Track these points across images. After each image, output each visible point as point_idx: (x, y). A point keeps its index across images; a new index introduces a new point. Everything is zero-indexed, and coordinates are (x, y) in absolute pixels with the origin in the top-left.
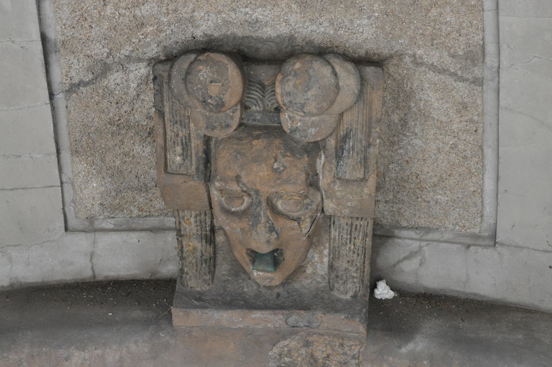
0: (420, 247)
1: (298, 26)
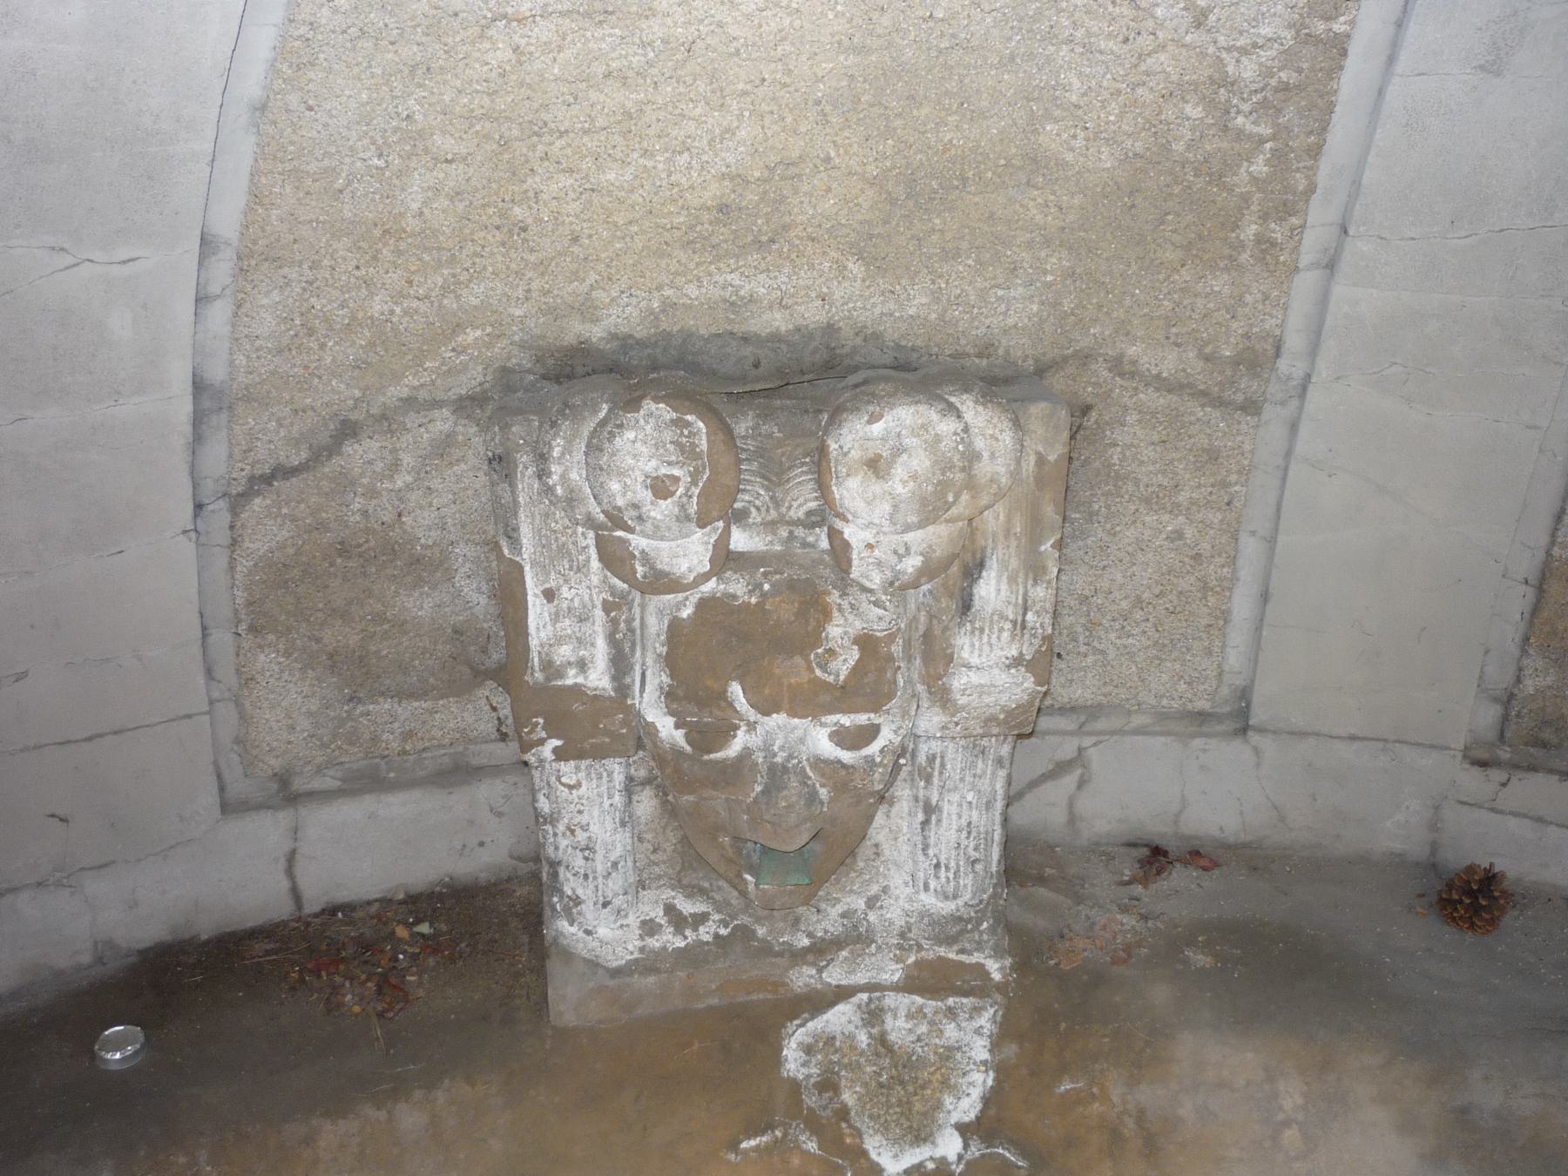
0: (1080, 750)
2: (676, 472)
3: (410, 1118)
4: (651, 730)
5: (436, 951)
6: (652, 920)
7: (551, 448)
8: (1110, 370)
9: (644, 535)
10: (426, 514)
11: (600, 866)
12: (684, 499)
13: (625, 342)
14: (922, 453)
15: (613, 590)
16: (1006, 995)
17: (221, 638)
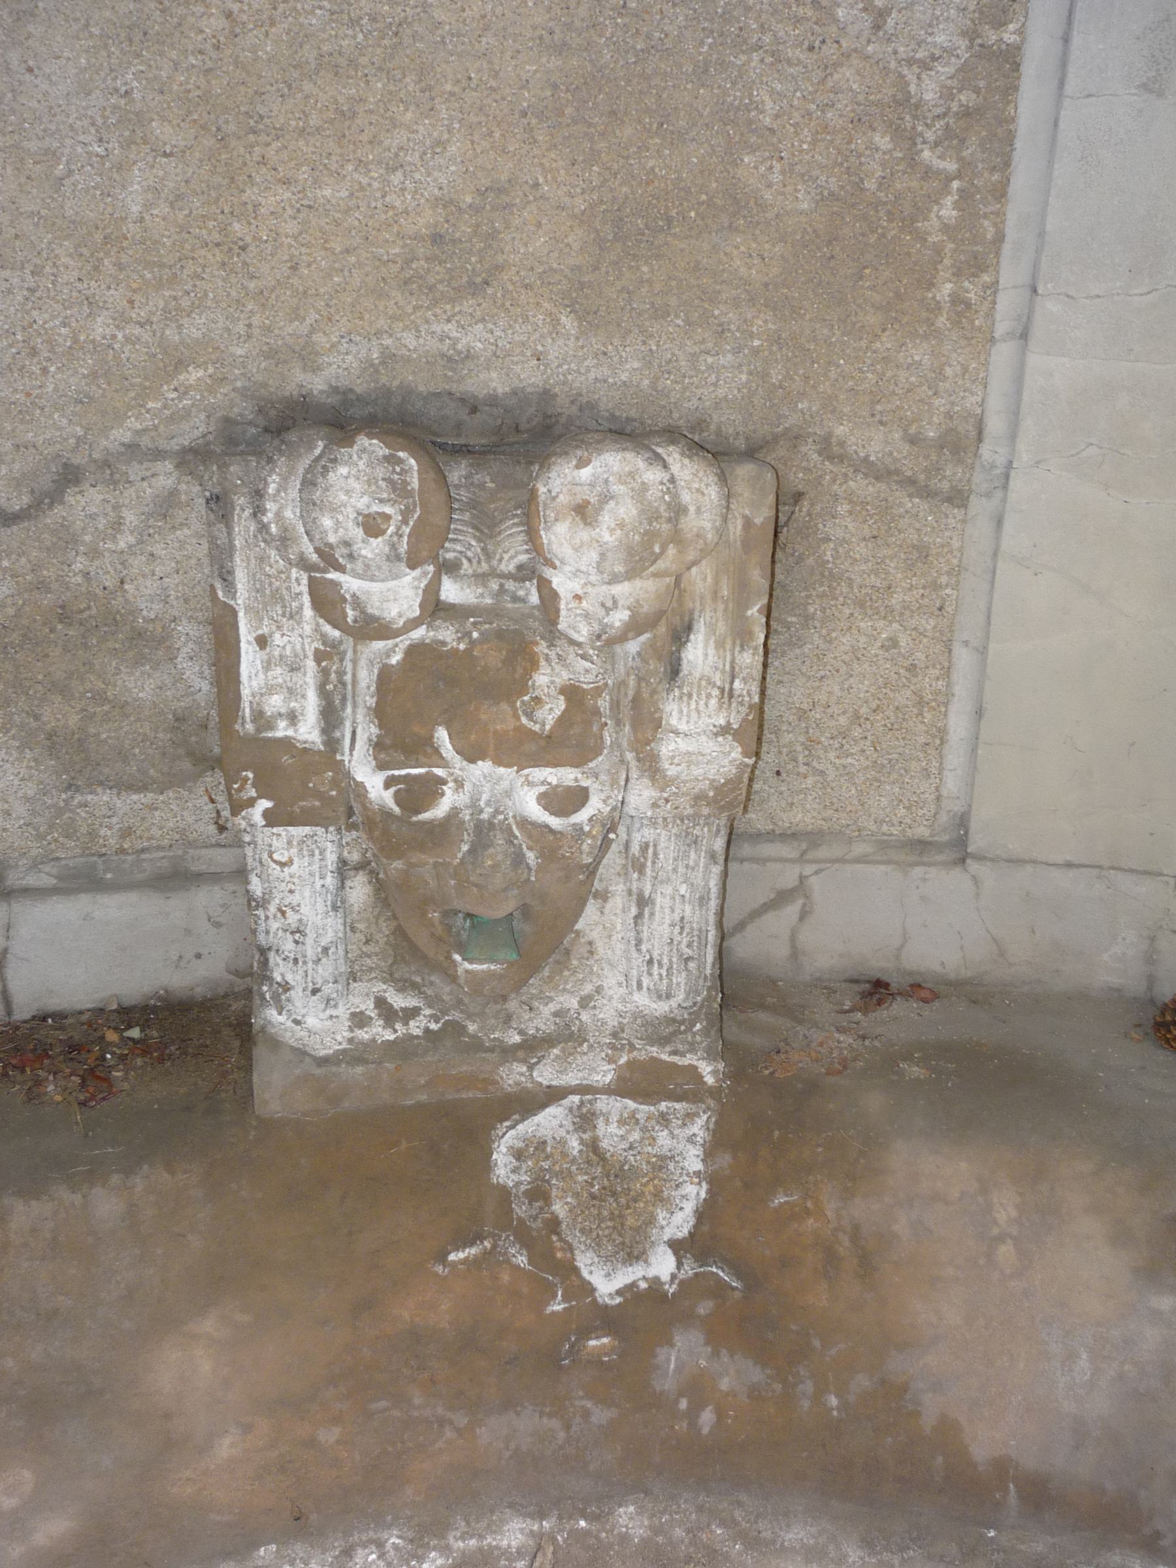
0: (802, 879)
1: (565, 367)
2: (388, 510)
3: (106, 1204)
5: (145, 1052)
6: (362, 1013)
7: (266, 484)
8: (820, 455)
9: (357, 575)
10: (148, 583)
11: (310, 951)
12: (395, 539)
13: (345, 395)
14: (629, 501)
15: (324, 637)
16: (719, 1100)
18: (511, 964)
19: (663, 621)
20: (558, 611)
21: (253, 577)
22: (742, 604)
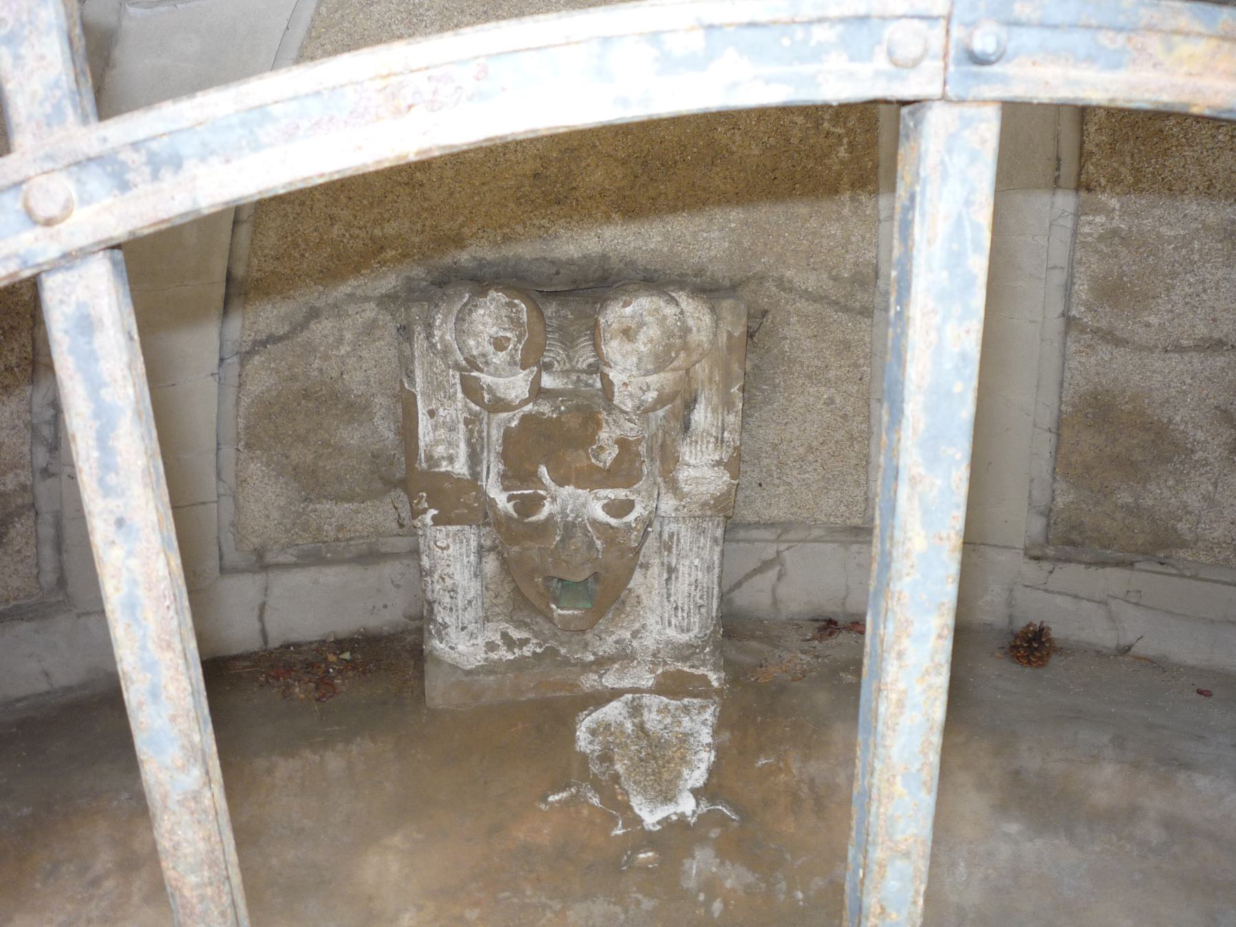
0: (778, 553)
2: (509, 335)
3: (334, 762)
4: (492, 503)
5: (354, 669)
15: (470, 411)
16: (721, 697)
17: (228, 452)
18: (587, 610)
19: (679, 397)
20: (613, 393)
21: (426, 374)
22: (727, 385)
